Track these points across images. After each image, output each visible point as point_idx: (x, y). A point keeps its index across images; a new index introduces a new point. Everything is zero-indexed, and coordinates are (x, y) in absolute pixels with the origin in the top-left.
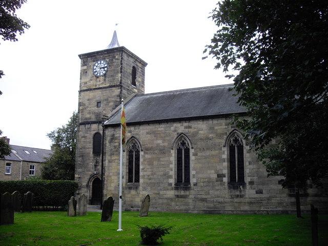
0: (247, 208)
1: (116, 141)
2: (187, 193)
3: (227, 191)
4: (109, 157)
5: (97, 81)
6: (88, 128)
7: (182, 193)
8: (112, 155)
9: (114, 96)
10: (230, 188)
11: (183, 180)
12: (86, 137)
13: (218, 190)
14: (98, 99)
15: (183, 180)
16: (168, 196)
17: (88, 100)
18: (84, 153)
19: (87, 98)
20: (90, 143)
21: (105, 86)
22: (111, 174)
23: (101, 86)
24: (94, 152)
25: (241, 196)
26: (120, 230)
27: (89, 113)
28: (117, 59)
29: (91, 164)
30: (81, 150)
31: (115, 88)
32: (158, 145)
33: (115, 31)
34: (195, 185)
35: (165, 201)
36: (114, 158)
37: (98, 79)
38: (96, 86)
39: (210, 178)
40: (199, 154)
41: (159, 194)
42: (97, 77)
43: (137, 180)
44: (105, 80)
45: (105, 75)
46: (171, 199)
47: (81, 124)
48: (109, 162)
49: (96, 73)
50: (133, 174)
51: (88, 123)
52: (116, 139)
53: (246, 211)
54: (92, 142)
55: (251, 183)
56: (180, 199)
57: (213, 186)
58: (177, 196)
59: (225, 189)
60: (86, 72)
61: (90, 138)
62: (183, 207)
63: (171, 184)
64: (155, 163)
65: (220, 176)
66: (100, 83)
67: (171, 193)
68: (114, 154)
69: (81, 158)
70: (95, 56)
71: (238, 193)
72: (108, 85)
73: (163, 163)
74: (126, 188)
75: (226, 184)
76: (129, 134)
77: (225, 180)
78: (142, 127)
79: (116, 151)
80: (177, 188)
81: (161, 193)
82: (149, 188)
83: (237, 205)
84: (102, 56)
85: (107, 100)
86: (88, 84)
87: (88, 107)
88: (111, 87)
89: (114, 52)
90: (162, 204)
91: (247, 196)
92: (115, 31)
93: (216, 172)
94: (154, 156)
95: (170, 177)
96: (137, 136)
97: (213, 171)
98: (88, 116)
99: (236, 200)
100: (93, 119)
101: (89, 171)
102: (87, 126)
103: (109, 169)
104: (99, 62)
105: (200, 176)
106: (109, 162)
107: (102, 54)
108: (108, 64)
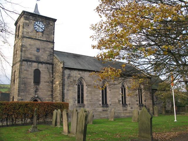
0: (128, 115)
1: (71, 78)
2: (107, 109)
3: (122, 108)
4: (67, 88)
5: (37, 35)
6: (30, 65)
7: (105, 109)
8: (68, 86)
9: (50, 48)
10: (123, 106)
11: (105, 103)
12: (28, 70)
13: (118, 107)
14: (38, 46)
15: (105, 103)
16: (99, 110)
17: (30, 45)
18: (27, 82)
19: (29, 43)
20: (31, 75)
21: (43, 39)
22: (69, 98)
23: (40, 39)
24: (35, 82)
25: (126, 110)
26: (175, 121)
27: (31, 54)
28: (51, 25)
29: (32, 90)
30: (24, 80)
31: (50, 43)
32: (94, 84)
33: (37, 4)
34: (110, 105)
35: (98, 113)
36: (70, 88)
37: (38, 33)
38: (36, 37)
39: (116, 102)
40: (112, 90)
41: (95, 109)
42: (37, 32)
43: (83, 102)
44: (43, 35)
45: (43, 32)
46: (101, 112)
47: (24, 60)
48: (67, 90)
49: (36, 29)
50: (80, 99)
51: (30, 61)
52: (71, 77)
53: (128, 116)
54: (33, 75)
55: (129, 104)
56: (104, 112)
57: (117, 106)
58: (103, 111)
59: (121, 107)
60: (28, 25)
61: (31, 72)
62: (106, 116)
63: (100, 105)
64: (93, 93)
65: (119, 101)
66: (39, 36)
67: (101, 109)
68: (70, 86)
69: (23, 85)
70: (36, 17)
71: (125, 109)
72: (45, 39)
73: (96, 93)
74: (78, 107)
75: (121, 104)
76: (79, 75)
77: (121, 103)
78: (86, 73)
79: (72, 84)
80: (103, 107)
81: (96, 109)
82: (90, 107)
83: (125, 114)
84: (41, 19)
85: (44, 49)
86: (30, 34)
87: (29, 50)
88: (47, 41)
89: (50, 20)
90: (97, 115)
91: (128, 110)
92: (37, 4)
93: (118, 99)
94: (92, 89)
95: (100, 101)
96: (83, 77)
97: (117, 99)
98: (29, 56)
99: (125, 111)
100: (34, 59)
101: (31, 95)
102: (29, 63)
103: (67, 95)
104: (39, 22)
105: (112, 100)
106: (67, 90)
107: (41, 18)
108: (45, 26)
